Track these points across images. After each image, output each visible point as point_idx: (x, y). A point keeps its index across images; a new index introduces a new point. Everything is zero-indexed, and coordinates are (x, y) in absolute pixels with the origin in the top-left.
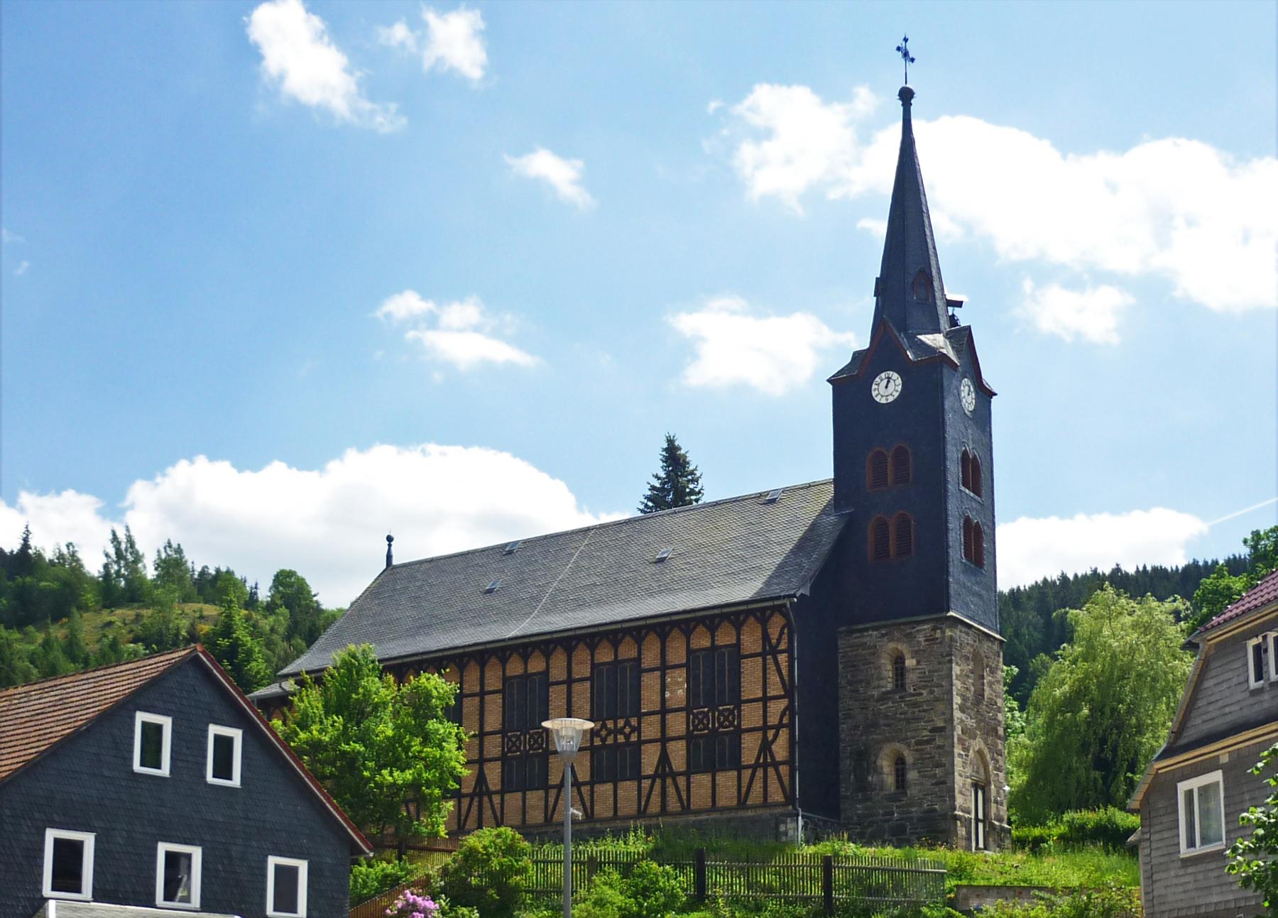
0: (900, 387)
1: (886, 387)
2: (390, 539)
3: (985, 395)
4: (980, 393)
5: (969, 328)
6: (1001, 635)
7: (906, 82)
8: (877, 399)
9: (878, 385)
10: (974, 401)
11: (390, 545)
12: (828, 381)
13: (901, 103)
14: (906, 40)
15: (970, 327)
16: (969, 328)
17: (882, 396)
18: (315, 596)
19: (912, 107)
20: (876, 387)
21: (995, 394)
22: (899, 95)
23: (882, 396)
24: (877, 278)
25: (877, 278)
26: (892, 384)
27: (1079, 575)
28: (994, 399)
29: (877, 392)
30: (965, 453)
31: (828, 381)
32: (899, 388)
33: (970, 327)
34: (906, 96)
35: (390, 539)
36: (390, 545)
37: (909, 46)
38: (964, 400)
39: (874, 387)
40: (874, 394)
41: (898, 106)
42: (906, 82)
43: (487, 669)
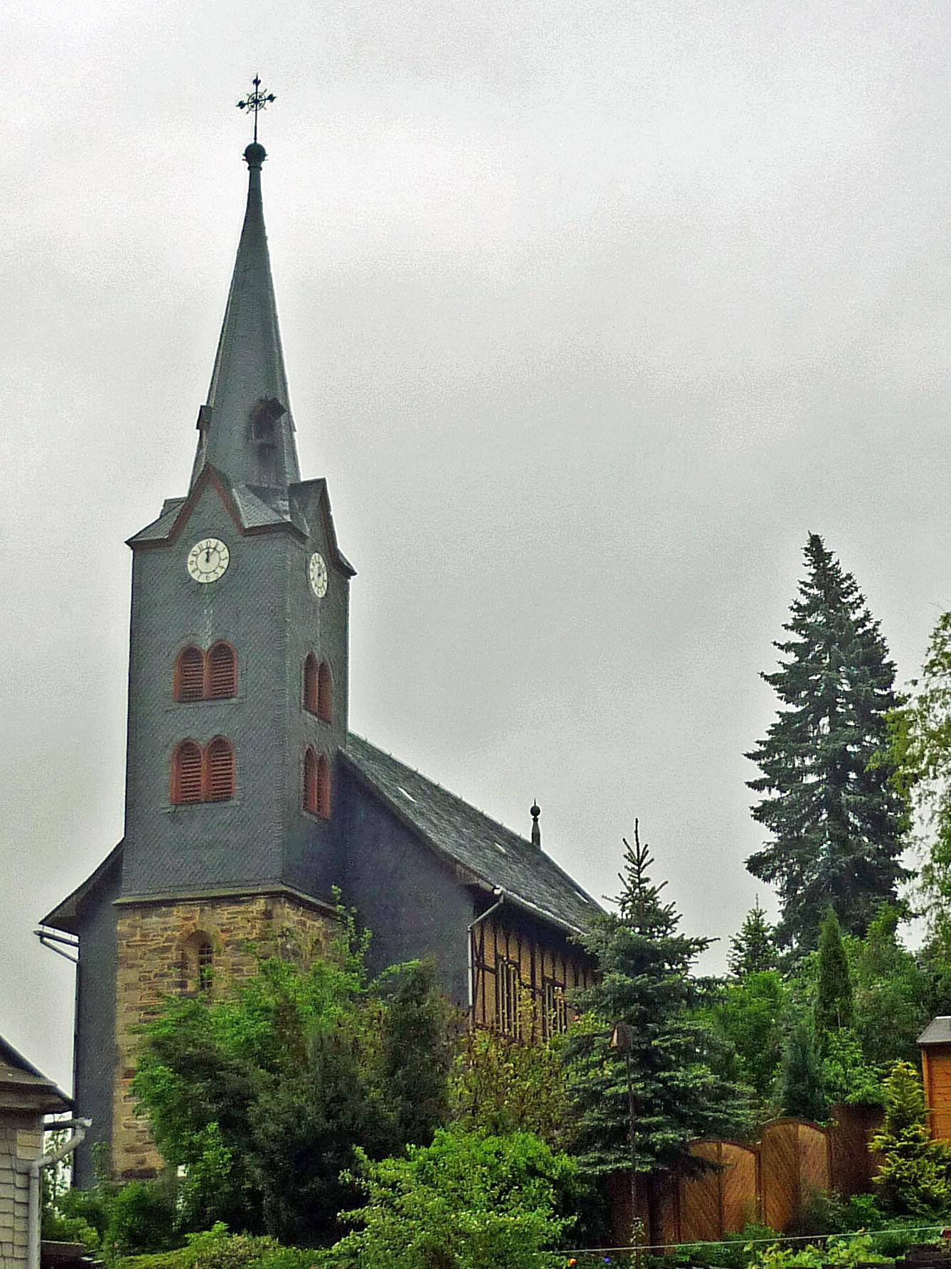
0: (227, 561)
1: (207, 560)
2: (535, 811)
3: (341, 571)
4: (334, 571)
5: (321, 483)
6: (721, 1240)
7: (255, 139)
10: (325, 584)
11: (535, 820)
12: (126, 542)
13: (247, 165)
14: (257, 82)
15: (324, 480)
16: (321, 483)
17: (201, 573)
18: (770, 790)
19: (262, 173)
20: (194, 559)
21: (355, 574)
22: (245, 155)
24: (352, 573)
25: (352, 573)
26: (214, 558)
27: (763, 838)
29: (194, 566)
30: (310, 658)
31: (126, 542)
32: (225, 564)
33: (324, 480)
34: (255, 155)
35: (535, 811)
36: (535, 820)
38: (313, 583)
39: (190, 558)
40: (190, 568)
41: (243, 168)
42: (255, 139)
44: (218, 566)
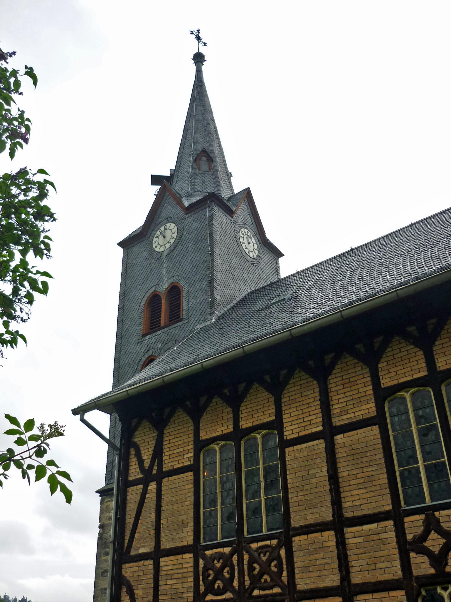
8: (157, 249)
9: (158, 237)
23: (161, 246)
28: (281, 260)
29: (157, 243)
37: (200, 35)
40: (154, 245)
43: (333, 383)
44: (168, 242)
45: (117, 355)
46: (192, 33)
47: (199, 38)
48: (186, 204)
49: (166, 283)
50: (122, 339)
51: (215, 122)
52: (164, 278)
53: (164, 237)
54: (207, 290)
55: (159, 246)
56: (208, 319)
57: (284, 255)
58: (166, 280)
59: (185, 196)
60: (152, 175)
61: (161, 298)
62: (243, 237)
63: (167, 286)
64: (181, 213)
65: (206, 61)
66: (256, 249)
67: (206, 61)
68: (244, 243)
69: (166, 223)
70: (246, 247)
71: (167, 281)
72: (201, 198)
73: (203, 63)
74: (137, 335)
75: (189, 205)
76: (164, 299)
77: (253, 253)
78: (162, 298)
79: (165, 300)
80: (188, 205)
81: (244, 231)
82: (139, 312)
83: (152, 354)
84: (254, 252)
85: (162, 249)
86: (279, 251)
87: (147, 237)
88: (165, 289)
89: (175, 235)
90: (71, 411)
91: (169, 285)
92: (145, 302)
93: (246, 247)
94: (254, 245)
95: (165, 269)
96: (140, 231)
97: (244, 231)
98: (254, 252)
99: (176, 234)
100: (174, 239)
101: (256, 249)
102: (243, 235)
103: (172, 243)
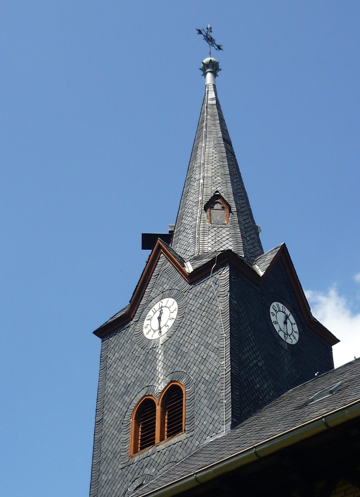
29: (149, 328)
45: (94, 472)
46: (200, 32)
47: (210, 40)
48: (189, 268)
49: (161, 382)
50: (101, 464)
51: (234, 156)
52: (159, 376)
53: (160, 332)
54: (221, 388)
55: (152, 331)
56: (222, 430)
57: (339, 341)
58: (162, 378)
59: (190, 260)
60: (143, 234)
61: (155, 404)
62: (275, 314)
63: (163, 387)
64: (183, 283)
65: (221, 70)
66: (295, 332)
67: (221, 70)
68: (276, 323)
69: (162, 299)
70: (280, 328)
71: (163, 380)
72: (210, 259)
73: (218, 74)
74: (121, 451)
75: (194, 270)
76: (160, 405)
77: (291, 337)
78: (157, 403)
79: (161, 406)
80: (193, 270)
81: (278, 305)
82: (124, 425)
83: (143, 482)
84: (293, 336)
85: (156, 336)
86: (332, 335)
87: (134, 320)
88: (160, 391)
89: (174, 315)
90: (93, 334)
91: (166, 385)
92: (132, 410)
93: (280, 328)
94: (293, 325)
95: (160, 363)
96: (125, 312)
97: (278, 305)
98: (293, 336)
99: (176, 312)
100: (174, 320)
101: (295, 332)
102: (276, 311)
103: (170, 326)
